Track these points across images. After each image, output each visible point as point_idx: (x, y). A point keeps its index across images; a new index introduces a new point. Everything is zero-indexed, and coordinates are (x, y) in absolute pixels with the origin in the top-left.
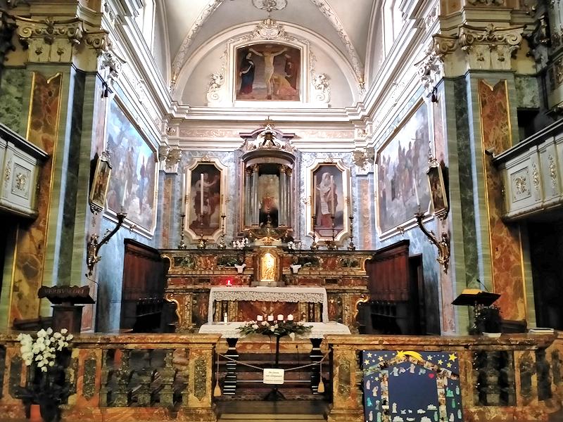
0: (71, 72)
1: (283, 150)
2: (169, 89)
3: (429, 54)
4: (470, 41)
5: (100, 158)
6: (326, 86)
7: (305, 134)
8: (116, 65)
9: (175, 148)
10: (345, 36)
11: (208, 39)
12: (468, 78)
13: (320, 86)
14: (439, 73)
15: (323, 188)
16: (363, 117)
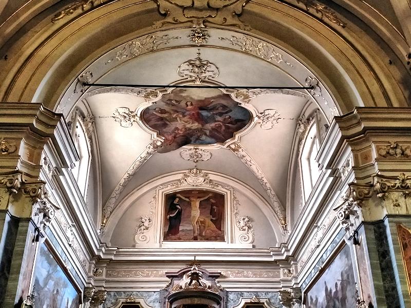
0: (6, 219)
1: (209, 291)
2: (99, 231)
3: (346, 200)
4: (385, 188)
5: (24, 302)
6: (249, 228)
7: (230, 274)
8: (50, 212)
9: (100, 289)
10: (266, 183)
11: (139, 186)
12: (386, 222)
13: (244, 228)
14: (358, 217)
16: (288, 257)
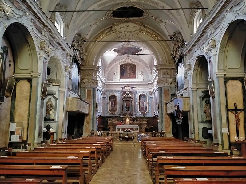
6: (142, 74)
15: (142, 100)
